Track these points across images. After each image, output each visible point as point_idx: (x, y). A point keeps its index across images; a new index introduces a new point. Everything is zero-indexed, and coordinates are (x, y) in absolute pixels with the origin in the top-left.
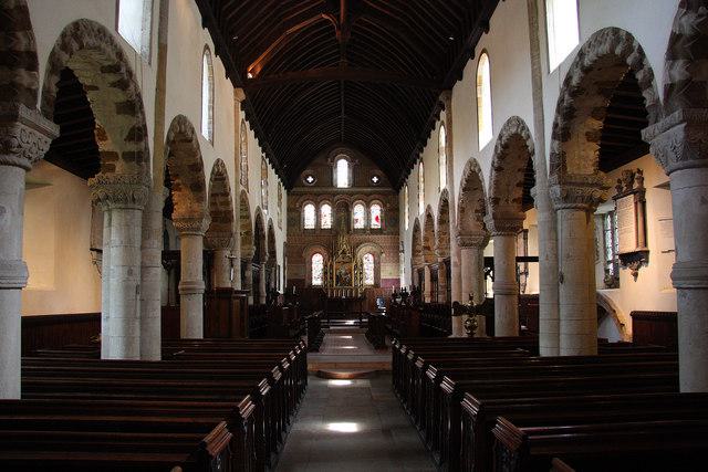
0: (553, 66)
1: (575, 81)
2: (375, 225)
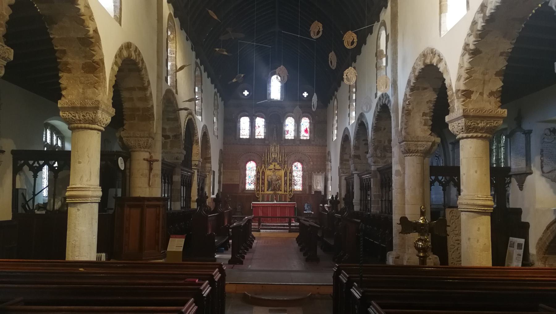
2: (305, 136)
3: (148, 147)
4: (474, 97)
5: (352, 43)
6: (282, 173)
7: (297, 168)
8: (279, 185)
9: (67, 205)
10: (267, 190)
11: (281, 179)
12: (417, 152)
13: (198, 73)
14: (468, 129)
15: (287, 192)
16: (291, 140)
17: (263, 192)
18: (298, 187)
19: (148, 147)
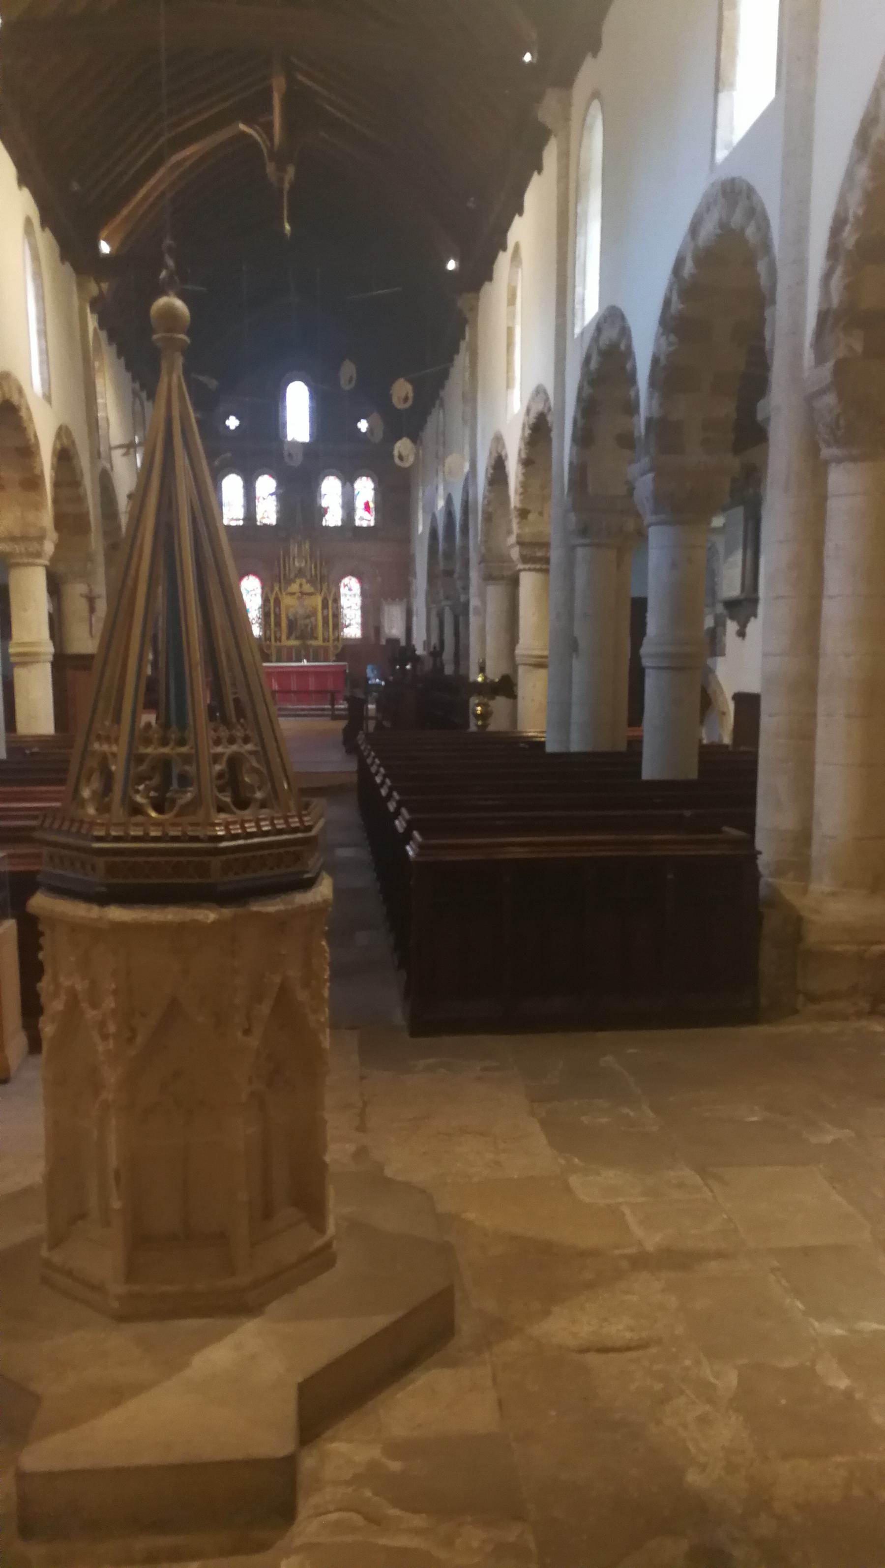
0: (578, 330)
1: (593, 365)
2: (364, 519)
3: (86, 576)
4: (531, 517)
5: (406, 399)
6: (318, 600)
7: (350, 590)
8: (312, 629)
9: (13, 665)
10: (288, 638)
11: (314, 613)
12: (502, 578)
13: (138, 407)
14: (525, 559)
15: (328, 641)
16: (336, 528)
17: (278, 643)
18: (353, 630)
19: (86, 576)
